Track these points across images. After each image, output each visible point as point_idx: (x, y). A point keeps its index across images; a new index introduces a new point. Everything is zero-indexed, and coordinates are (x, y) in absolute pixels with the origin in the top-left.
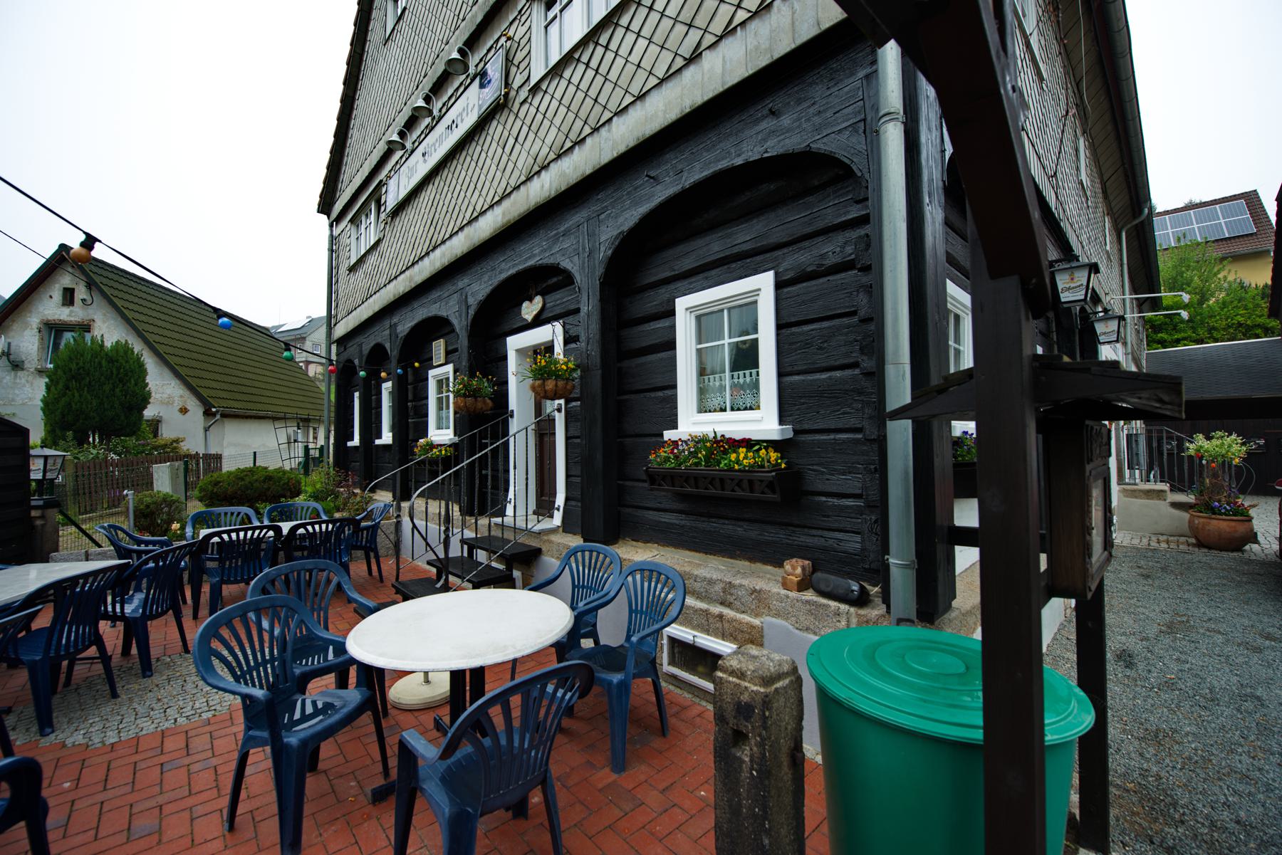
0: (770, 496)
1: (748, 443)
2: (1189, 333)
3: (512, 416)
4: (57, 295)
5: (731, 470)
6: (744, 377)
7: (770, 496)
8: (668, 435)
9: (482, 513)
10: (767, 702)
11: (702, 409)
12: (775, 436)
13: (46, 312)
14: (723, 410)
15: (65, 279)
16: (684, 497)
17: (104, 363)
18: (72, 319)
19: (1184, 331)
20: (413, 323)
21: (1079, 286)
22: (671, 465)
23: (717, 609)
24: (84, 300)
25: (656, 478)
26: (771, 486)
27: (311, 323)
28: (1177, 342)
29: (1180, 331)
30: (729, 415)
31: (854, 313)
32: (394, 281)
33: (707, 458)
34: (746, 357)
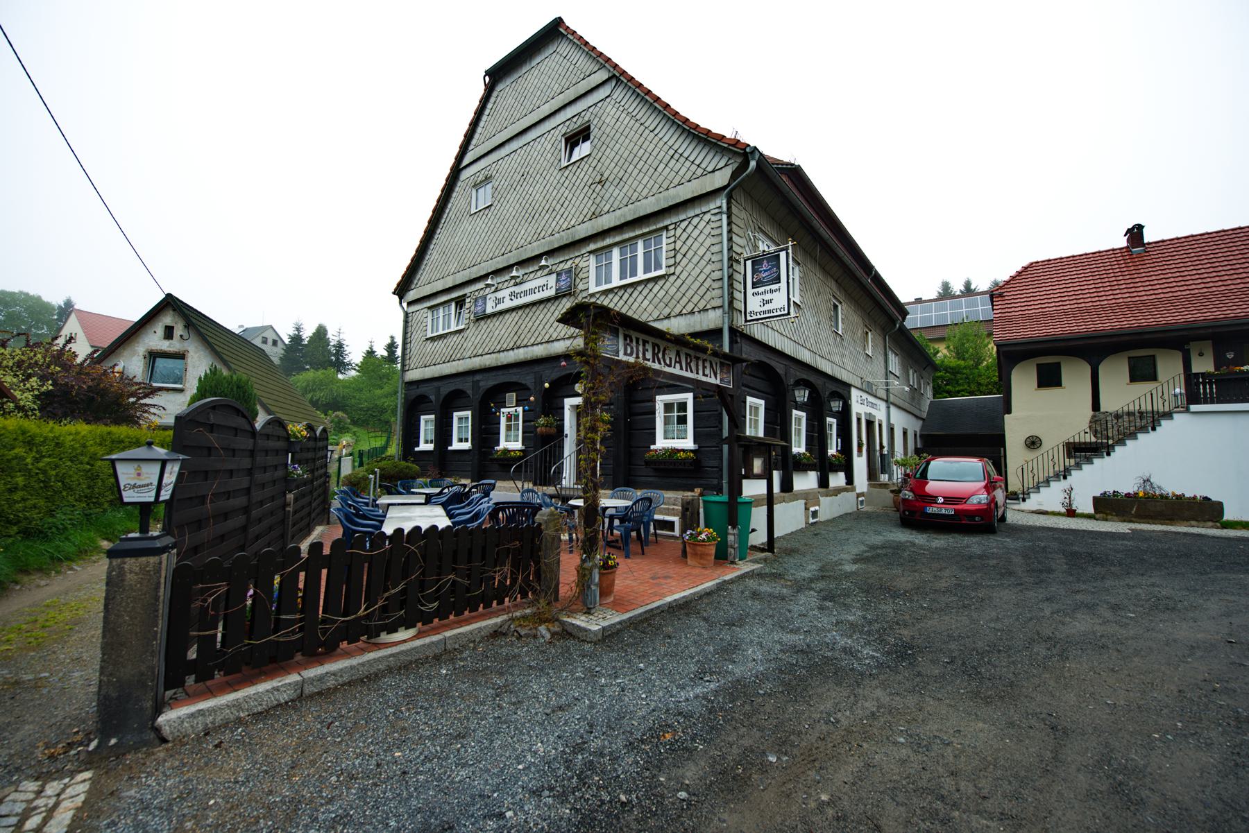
0: (691, 467)
1: (683, 451)
2: (966, 387)
3: (566, 437)
4: (160, 329)
5: (678, 459)
6: (681, 427)
7: (691, 467)
8: (652, 447)
9: (545, 485)
10: (693, 500)
11: (666, 438)
12: (692, 448)
13: (151, 343)
14: (674, 438)
15: (168, 319)
16: (656, 470)
17: (235, 389)
18: (171, 349)
19: (963, 385)
20: (495, 383)
21: (148, 485)
22: (655, 457)
23: (672, 507)
24: (181, 336)
25: (648, 463)
26: (691, 464)
27: (246, 332)
28: (957, 394)
29: (959, 385)
30: (676, 441)
31: (716, 411)
32: (480, 357)
33: (669, 455)
34: (682, 420)
